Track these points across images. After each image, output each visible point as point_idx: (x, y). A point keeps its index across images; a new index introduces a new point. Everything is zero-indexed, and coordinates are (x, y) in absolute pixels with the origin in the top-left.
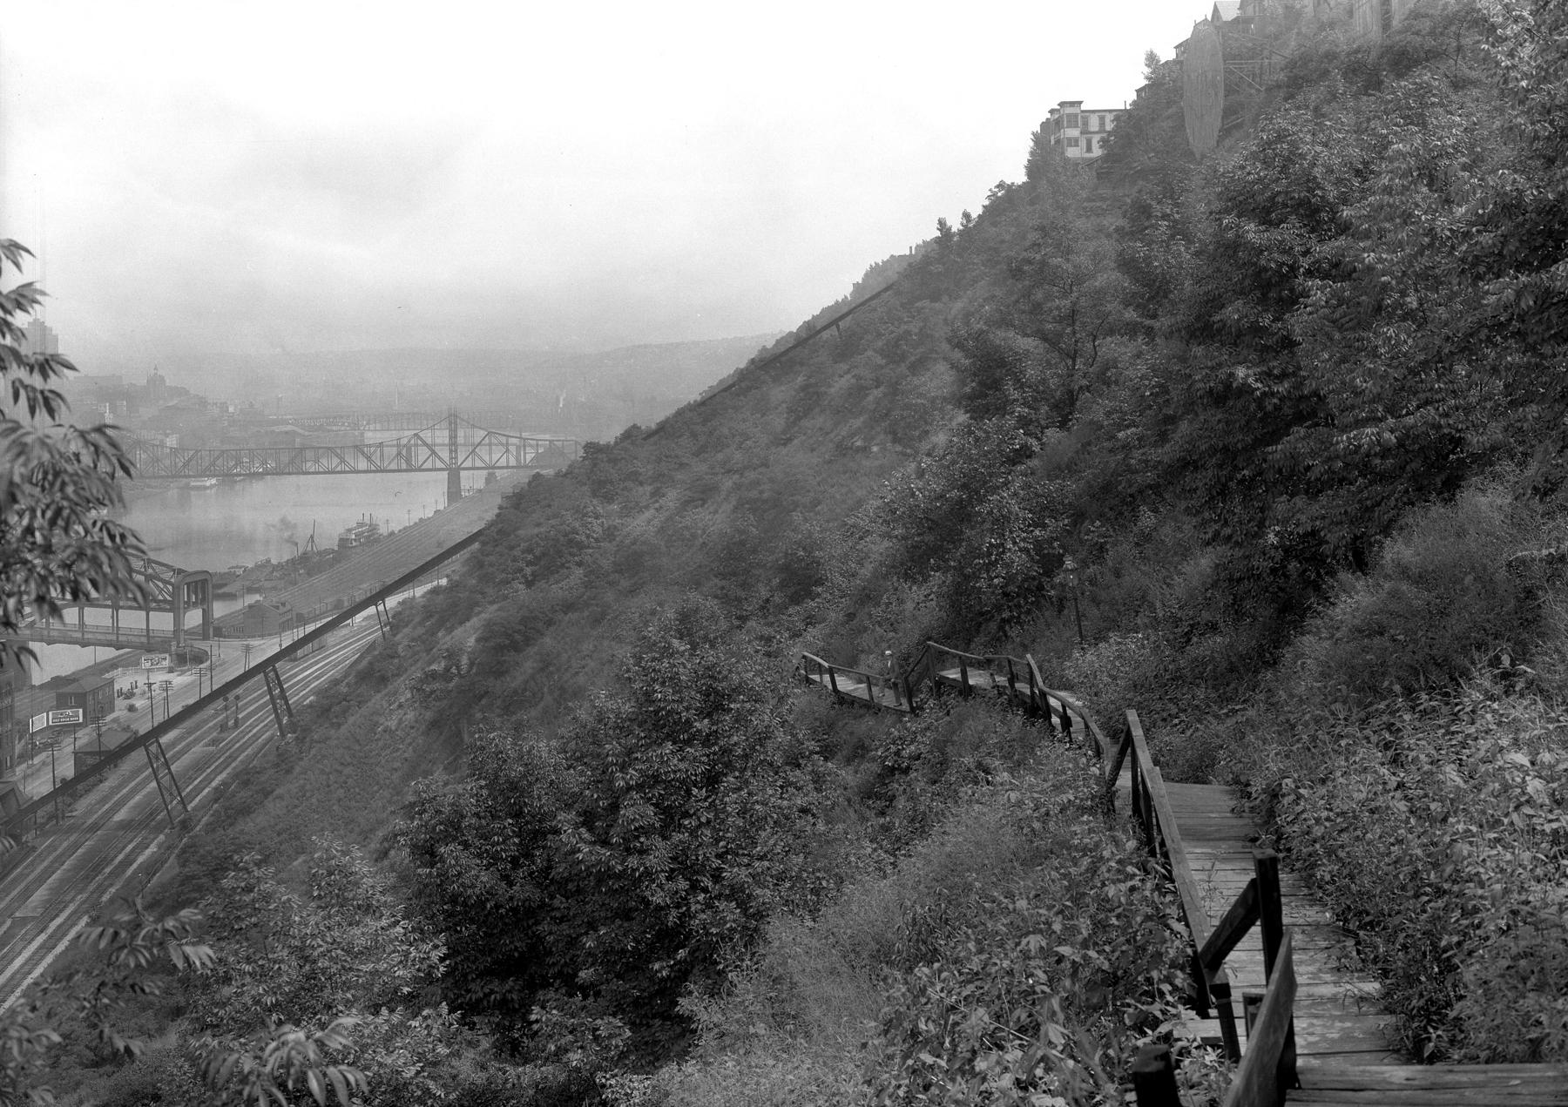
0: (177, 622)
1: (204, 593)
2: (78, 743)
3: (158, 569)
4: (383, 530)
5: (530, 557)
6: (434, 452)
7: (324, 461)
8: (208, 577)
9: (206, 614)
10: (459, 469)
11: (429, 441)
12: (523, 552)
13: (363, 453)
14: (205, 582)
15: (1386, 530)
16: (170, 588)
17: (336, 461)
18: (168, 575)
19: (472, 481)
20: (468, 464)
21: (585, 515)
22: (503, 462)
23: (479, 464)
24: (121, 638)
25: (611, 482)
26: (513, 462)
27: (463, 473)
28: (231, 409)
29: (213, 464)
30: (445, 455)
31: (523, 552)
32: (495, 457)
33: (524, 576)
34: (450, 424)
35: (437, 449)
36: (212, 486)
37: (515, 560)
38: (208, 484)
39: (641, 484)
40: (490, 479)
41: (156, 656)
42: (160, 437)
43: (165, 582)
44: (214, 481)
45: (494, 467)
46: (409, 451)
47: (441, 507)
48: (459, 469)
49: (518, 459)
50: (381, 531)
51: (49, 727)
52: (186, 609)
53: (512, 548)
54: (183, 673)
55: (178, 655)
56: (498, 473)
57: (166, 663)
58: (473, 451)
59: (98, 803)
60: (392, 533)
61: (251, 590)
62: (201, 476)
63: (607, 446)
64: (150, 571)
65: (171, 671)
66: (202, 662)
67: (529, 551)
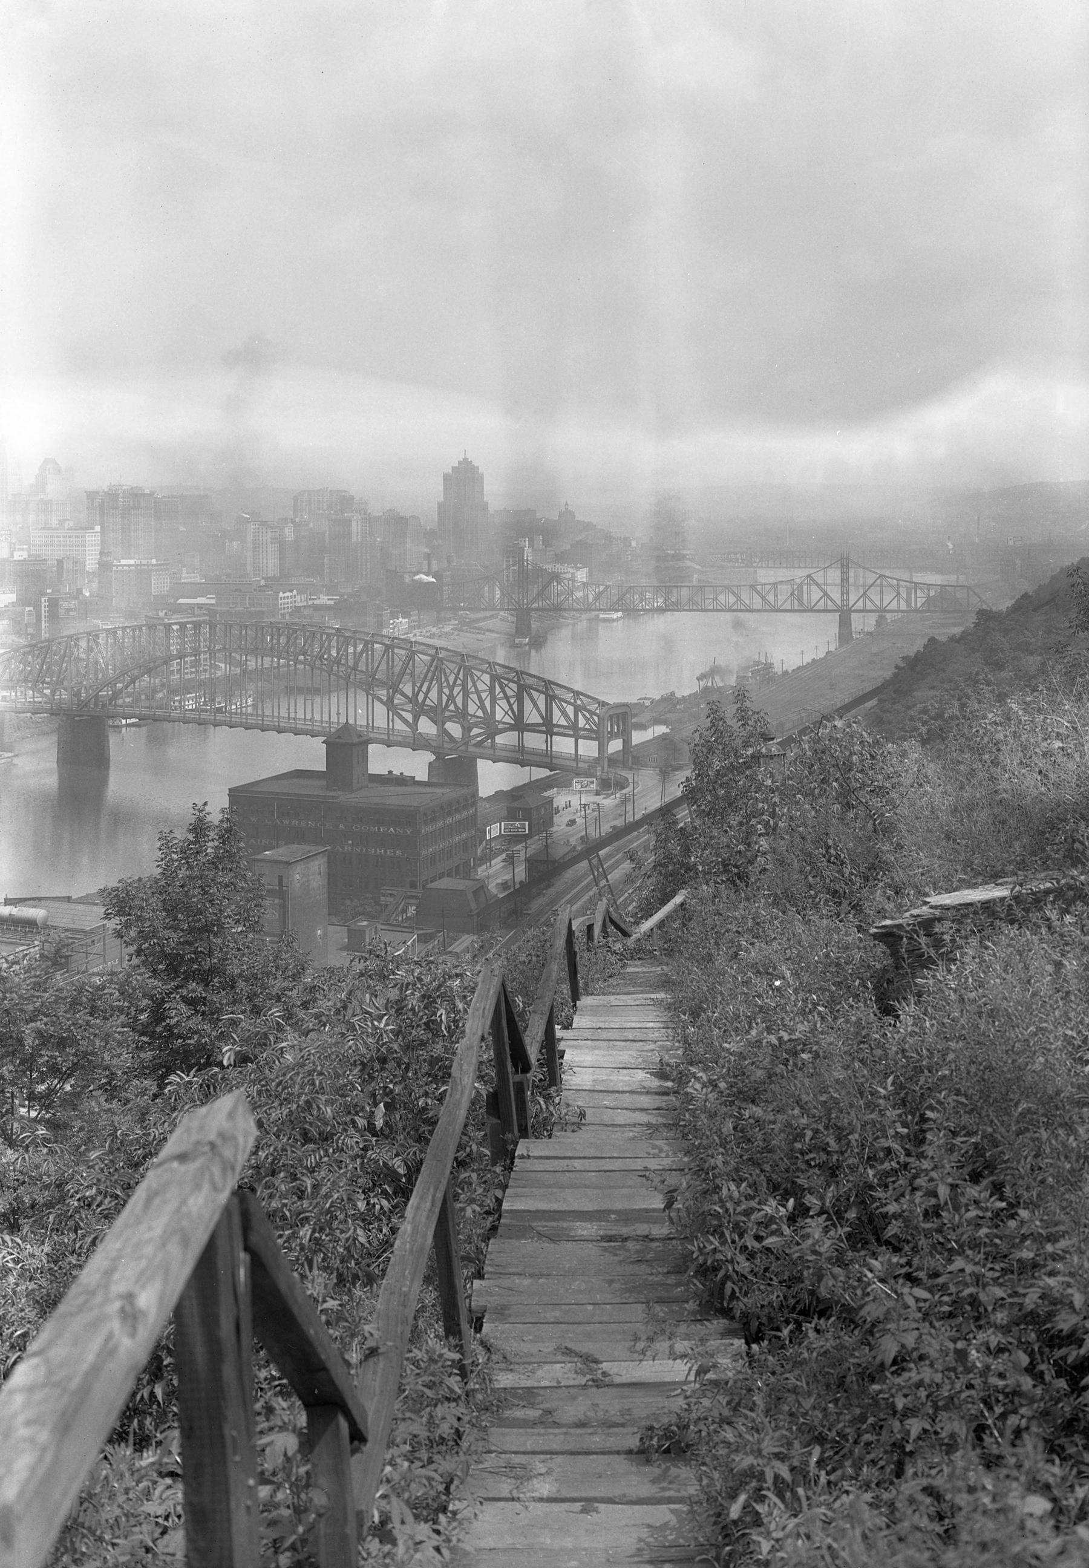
0: (602, 748)
1: (624, 724)
2: (530, 851)
3: (586, 700)
4: (778, 669)
5: (925, 717)
6: (826, 594)
7: (722, 598)
8: (628, 710)
9: (627, 742)
10: (850, 611)
11: (820, 581)
12: (919, 713)
13: (758, 592)
14: (625, 714)
15: (157, 881)
16: (596, 719)
17: (732, 599)
18: (593, 707)
19: (863, 624)
20: (860, 605)
21: (977, 682)
22: (894, 606)
23: (869, 606)
24: (581, 765)
25: (1003, 651)
26: (903, 606)
27: (854, 616)
28: (634, 544)
29: (621, 599)
30: (836, 595)
31: (919, 713)
32: (887, 599)
33: (920, 734)
34: (842, 566)
35: (829, 589)
36: (618, 619)
37: (912, 719)
38: (615, 616)
39: (1031, 654)
40: (880, 621)
41: (586, 780)
42: (572, 571)
43: (592, 713)
44: (620, 614)
45: (885, 611)
46: (801, 592)
47: (832, 649)
48: (850, 611)
49: (908, 604)
50: (776, 670)
51: (501, 835)
52: (610, 739)
53: (909, 708)
54: (608, 796)
55: (602, 779)
56: (888, 616)
57: (594, 786)
58: (865, 593)
59: (548, 905)
60: (786, 673)
61: (657, 721)
62: (610, 610)
63: (999, 614)
64: (579, 702)
65: (597, 793)
66: (623, 788)
67: (925, 711)
